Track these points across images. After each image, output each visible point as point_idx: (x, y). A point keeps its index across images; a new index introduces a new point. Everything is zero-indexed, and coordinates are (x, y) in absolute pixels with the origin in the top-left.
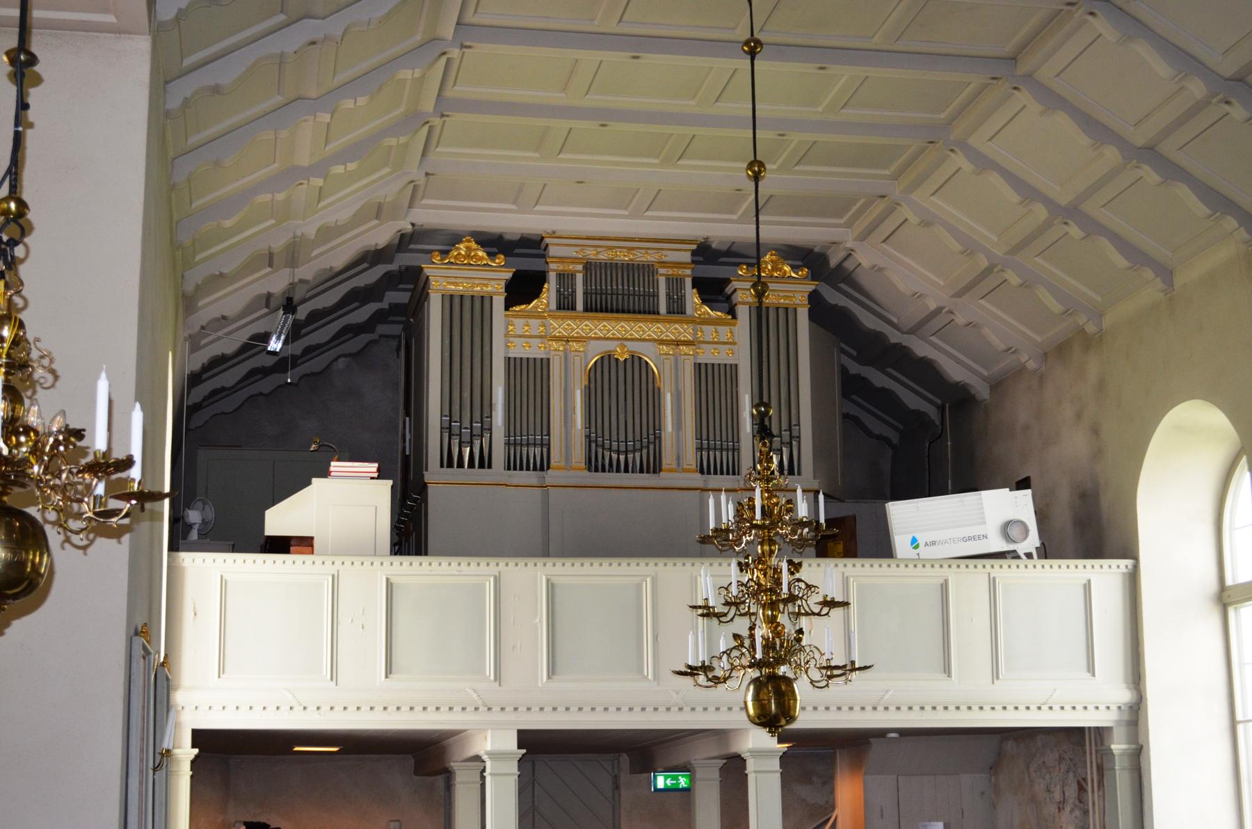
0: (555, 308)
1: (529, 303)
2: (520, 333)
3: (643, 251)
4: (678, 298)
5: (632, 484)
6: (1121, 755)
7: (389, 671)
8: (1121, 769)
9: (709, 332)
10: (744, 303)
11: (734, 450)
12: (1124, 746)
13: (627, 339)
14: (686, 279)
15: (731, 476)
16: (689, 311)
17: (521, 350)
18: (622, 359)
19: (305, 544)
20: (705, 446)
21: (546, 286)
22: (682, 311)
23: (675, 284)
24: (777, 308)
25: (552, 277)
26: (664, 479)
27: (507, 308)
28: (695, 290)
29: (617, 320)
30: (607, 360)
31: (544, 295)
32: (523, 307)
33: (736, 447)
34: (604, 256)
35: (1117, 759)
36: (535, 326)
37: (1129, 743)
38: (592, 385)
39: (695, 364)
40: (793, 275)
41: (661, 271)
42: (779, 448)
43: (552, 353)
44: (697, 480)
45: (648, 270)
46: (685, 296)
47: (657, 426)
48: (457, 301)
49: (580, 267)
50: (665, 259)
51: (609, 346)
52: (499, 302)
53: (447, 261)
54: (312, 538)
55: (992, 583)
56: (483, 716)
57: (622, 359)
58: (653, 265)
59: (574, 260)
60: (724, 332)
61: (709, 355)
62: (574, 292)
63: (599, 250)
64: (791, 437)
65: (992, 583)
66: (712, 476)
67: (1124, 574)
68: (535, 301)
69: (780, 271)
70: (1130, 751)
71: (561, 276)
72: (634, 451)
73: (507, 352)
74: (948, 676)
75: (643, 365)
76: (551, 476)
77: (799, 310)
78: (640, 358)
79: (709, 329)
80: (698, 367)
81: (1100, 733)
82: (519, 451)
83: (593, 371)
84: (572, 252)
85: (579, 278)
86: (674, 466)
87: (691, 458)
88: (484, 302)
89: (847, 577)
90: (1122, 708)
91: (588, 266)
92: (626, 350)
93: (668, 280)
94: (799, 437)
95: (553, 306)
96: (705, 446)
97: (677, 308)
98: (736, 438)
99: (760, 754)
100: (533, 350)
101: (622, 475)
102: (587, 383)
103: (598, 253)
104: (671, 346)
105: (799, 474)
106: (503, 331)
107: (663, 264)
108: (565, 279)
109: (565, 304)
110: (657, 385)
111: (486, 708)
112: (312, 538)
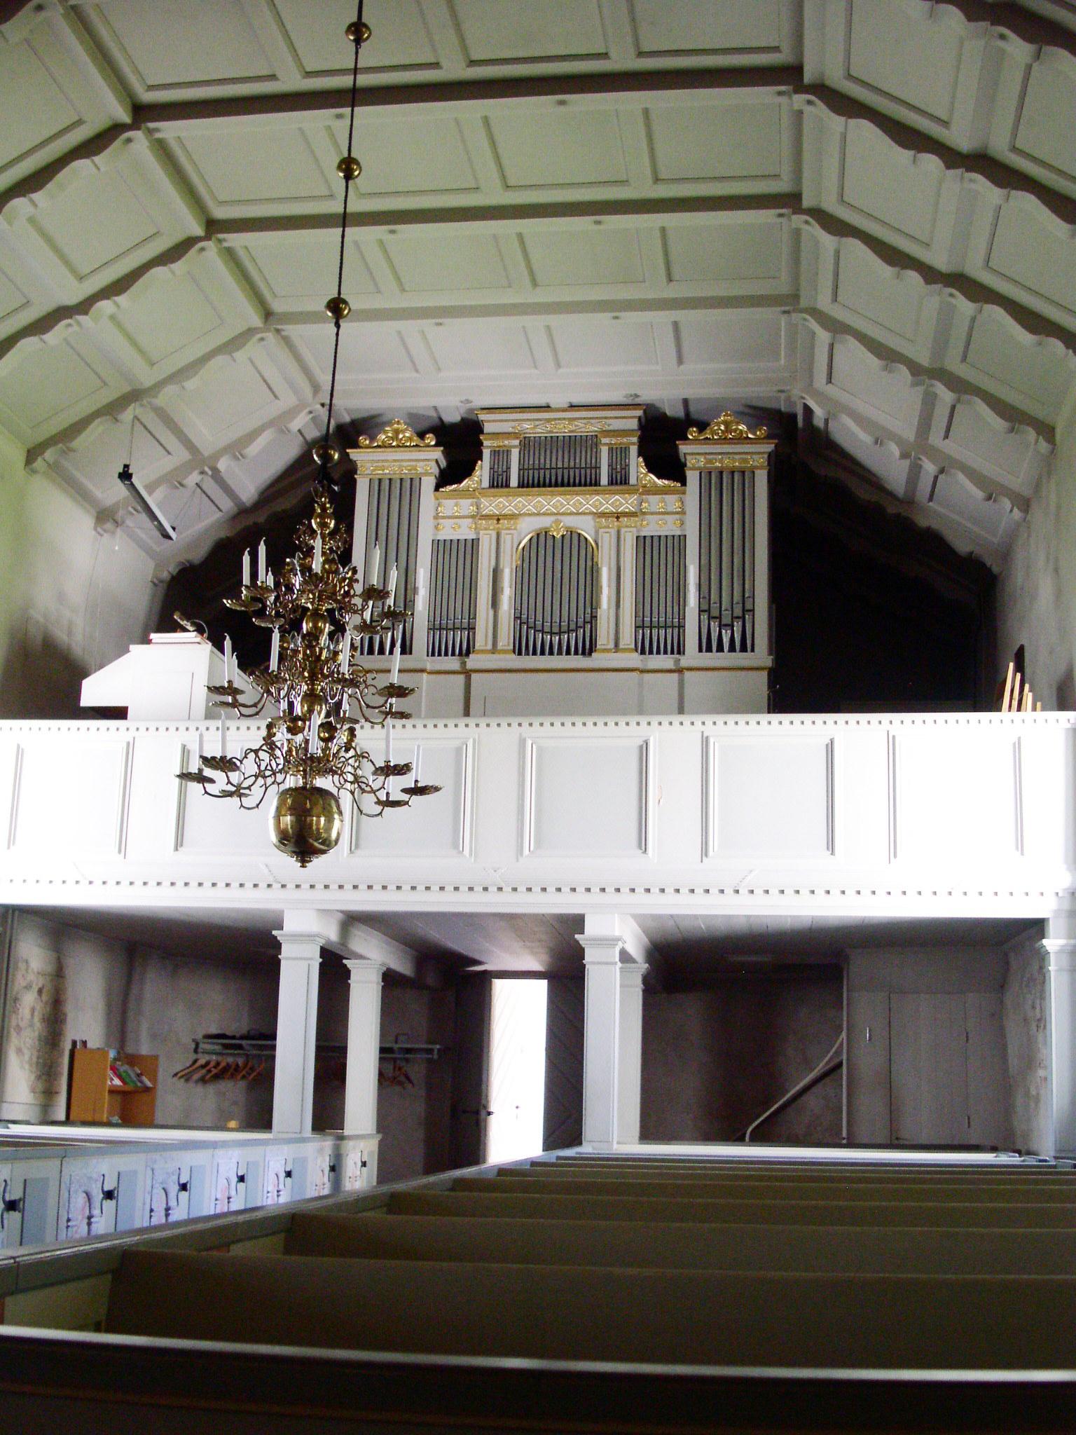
0: (487, 485)
1: (460, 482)
2: (449, 514)
3: (585, 421)
4: (621, 469)
5: (560, 666)
6: (1057, 953)
7: (179, 843)
8: (1057, 971)
9: (654, 503)
10: (693, 469)
11: (679, 627)
12: (1062, 942)
13: (563, 514)
14: (631, 447)
15: (669, 656)
16: (633, 481)
17: (448, 532)
18: (558, 536)
19: (118, 713)
20: (647, 623)
21: (479, 462)
22: (625, 481)
23: (619, 453)
24: (733, 473)
25: (486, 453)
26: (597, 660)
27: (437, 489)
28: (641, 459)
29: (553, 494)
30: (541, 539)
31: (477, 473)
32: (454, 486)
33: (681, 625)
34: (541, 431)
35: (1052, 958)
36: (466, 506)
37: (1069, 937)
38: (526, 565)
39: (637, 537)
40: (750, 436)
41: (604, 440)
42: (730, 623)
43: (481, 532)
44: (635, 660)
45: (591, 443)
46: (629, 465)
47: (594, 605)
48: (386, 484)
49: (516, 442)
50: (607, 428)
51: (545, 522)
52: (429, 483)
53: (376, 444)
54: (126, 708)
55: (892, 742)
56: (291, 893)
57: (558, 536)
58: (596, 436)
59: (514, 435)
60: (672, 502)
61: (653, 527)
62: (509, 468)
63: (537, 423)
64: (744, 610)
65: (892, 742)
66: (655, 656)
67: (1068, 729)
68: (467, 480)
69: (735, 432)
70: (1069, 948)
71: (495, 453)
72: (569, 631)
73: (435, 535)
74: (832, 854)
75: (582, 539)
76: (473, 662)
77: (757, 472)
78: (579, 534)
79: (654, 499)
80: (641, 541)
81: (1036, 927)
82: (459, 638)
83: (527, 549)
84: (507, 427)
85: (515, 454)
86: (612, 645)
87: (627, 638)
88: (411, 486)
89: (707, 737)
90: (1060, 895)
91: (527, 444)
92: (562, 524)
93: (611, 450)
94: (753, 610)
95: (486, 484)
96: (647, 623)
97: (620, 480)
98: (681, 617)
99: (599, 942)
100: (464, 532)
101: (564, 657)
102: (519, 563)
103: (536, 426)
104: (610, 519)
105: (753, 650)
106: (433, 513)
107: (608, 433)
108: (500, 455)
109: (499, 482)
110: (595, 560)
111: (280, 885)
112: (126, 708)
